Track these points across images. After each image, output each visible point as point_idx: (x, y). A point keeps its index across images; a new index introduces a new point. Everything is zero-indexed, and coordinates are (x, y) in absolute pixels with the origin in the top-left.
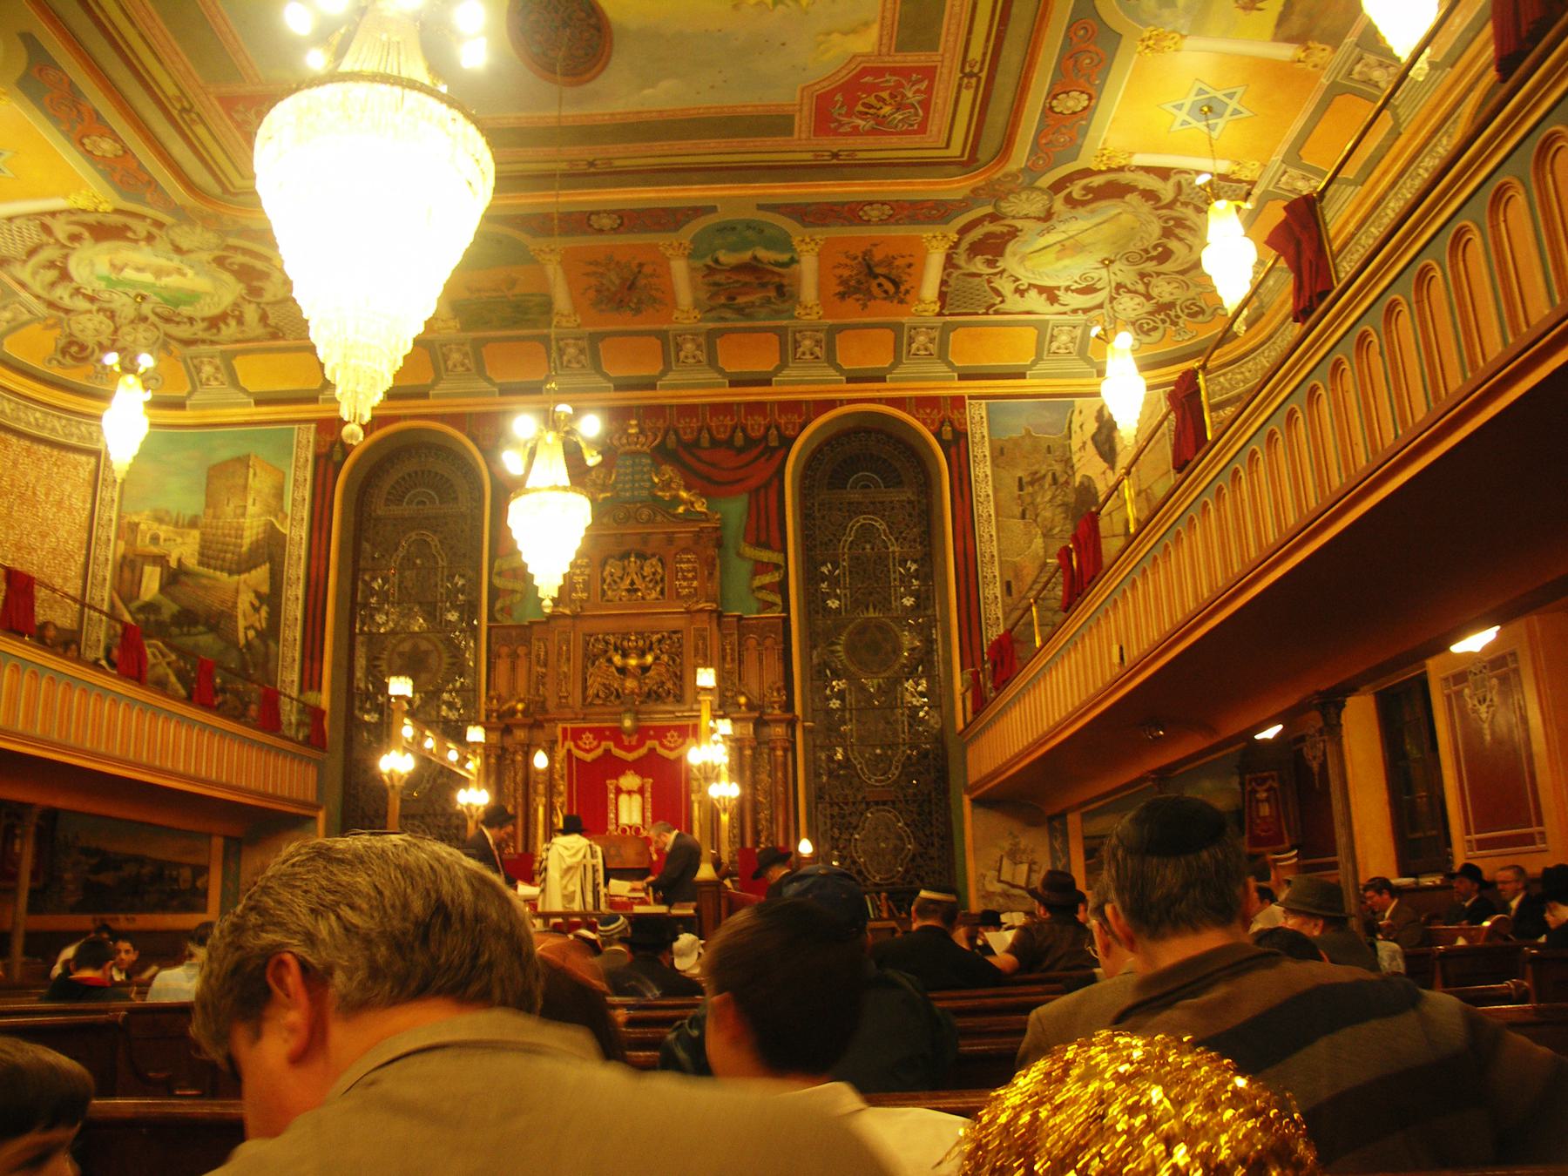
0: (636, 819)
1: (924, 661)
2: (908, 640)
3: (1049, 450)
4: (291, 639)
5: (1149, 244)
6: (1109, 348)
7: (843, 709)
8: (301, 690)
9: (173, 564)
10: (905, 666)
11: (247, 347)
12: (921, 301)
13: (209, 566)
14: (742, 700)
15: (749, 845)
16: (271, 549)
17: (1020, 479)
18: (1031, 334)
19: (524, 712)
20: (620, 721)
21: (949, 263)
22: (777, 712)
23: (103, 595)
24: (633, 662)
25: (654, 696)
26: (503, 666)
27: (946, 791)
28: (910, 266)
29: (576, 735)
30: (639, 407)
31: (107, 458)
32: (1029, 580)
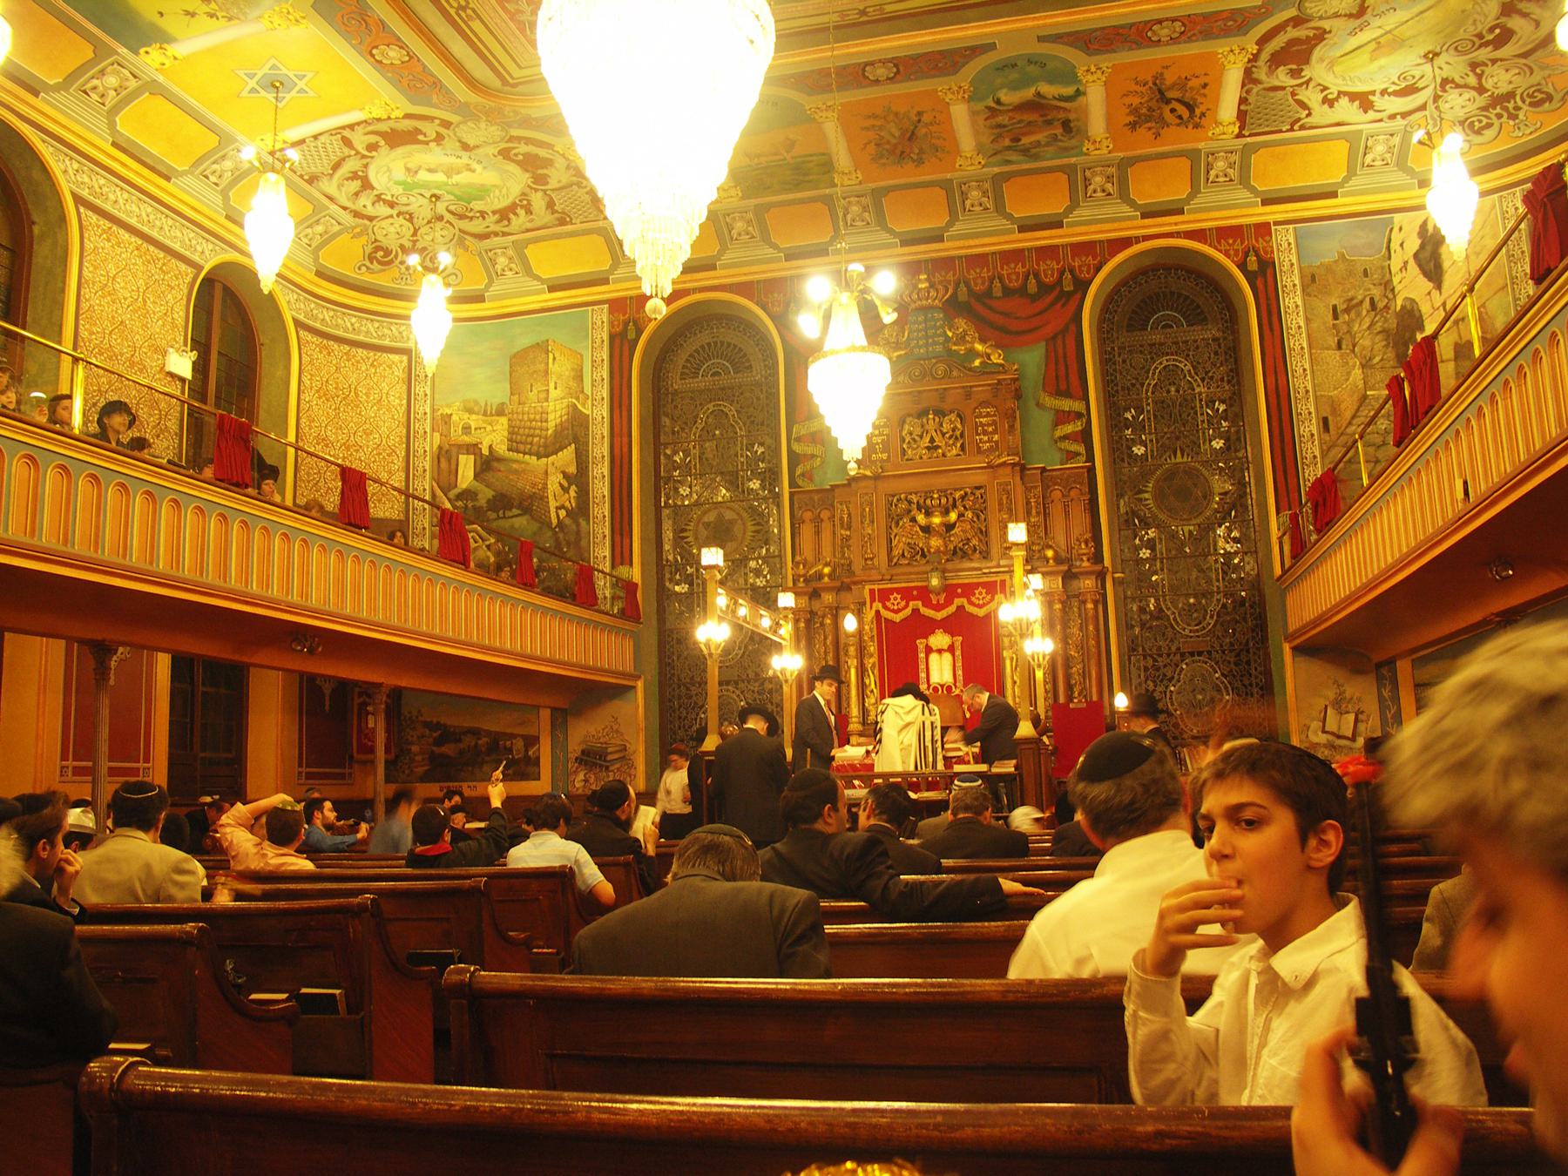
0: (947, 678)
1: (1237, 506)
2: (1221, 485)
3: (1365, 273)
4: (600, 516)
5: (1481, 28)
6: (1435, 154)
7: (1152, 559)
8: (613, 566)
9: (485, 452)
10: (1217, 511)
11: (537, 234)
12: (1218, 124)
13: (518, 451)
14: (1050, 553)
15: (1062, 700)
16: (574, 431)
17: (1335, 308)
18: (1342, 147)
19: (830, 575)
20: (927, 580)
21: (1249, 77)
22: (1086, 564)
23: (424, 485)
24: (937, 520)
25: (960, 553)
26: (807, 531)
27: (1265, 639)
28: (1205, 86)
29: (884, 596)
30: (926, 261)
31: (418, 356)
32: (1348, 414)
